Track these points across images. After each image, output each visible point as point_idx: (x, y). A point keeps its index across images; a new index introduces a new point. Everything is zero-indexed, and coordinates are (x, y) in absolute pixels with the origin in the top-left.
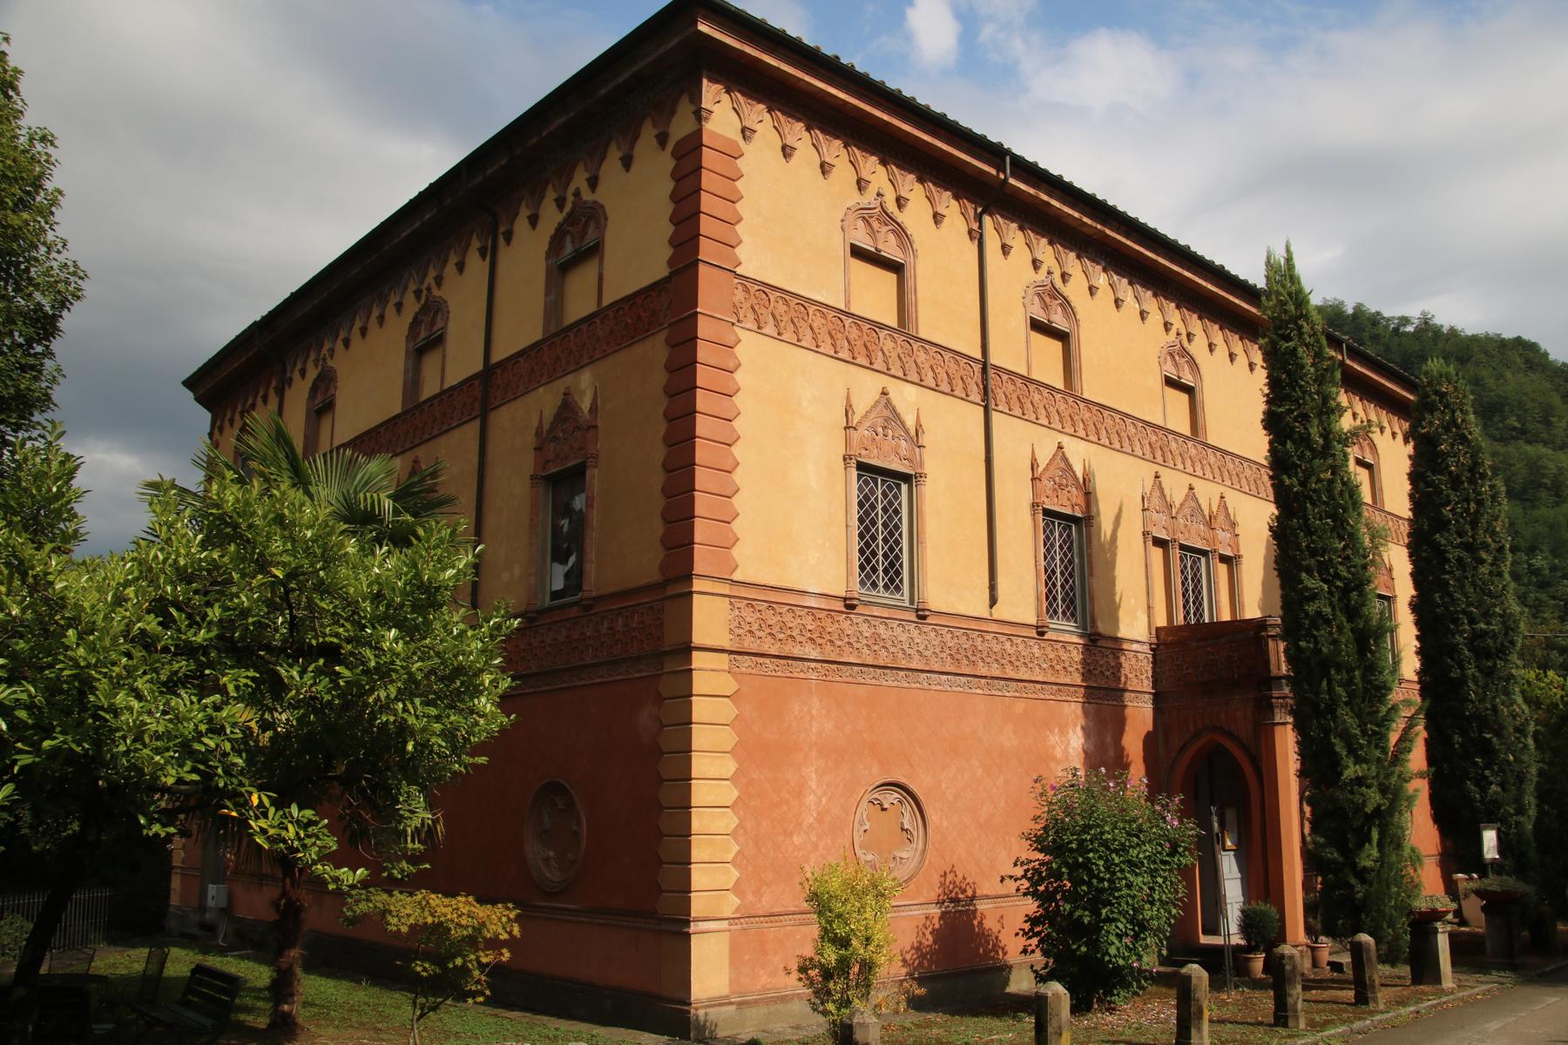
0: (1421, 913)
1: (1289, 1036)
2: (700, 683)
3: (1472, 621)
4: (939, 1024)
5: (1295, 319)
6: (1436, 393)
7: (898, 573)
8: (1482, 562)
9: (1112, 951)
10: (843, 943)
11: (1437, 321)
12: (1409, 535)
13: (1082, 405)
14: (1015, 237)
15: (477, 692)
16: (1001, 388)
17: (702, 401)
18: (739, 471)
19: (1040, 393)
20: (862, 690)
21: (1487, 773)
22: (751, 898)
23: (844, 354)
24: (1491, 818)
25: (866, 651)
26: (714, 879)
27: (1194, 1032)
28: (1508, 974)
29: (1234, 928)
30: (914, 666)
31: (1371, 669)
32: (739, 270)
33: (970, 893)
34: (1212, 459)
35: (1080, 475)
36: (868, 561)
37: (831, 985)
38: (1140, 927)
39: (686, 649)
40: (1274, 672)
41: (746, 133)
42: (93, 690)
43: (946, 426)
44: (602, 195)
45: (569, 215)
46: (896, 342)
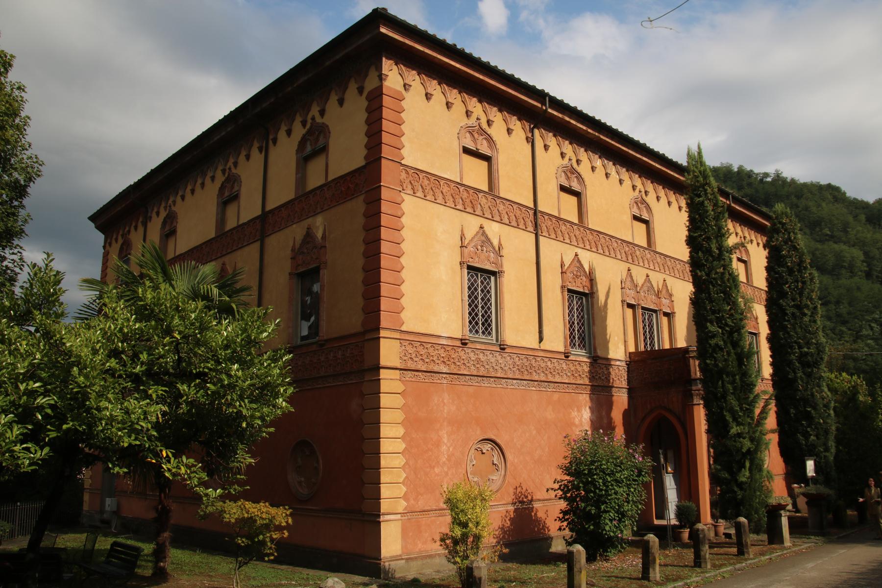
0: (773, 506)
1: (702, 572)
2: (384, 386)
3: (800, 347)
4: (514, 569)
5: (703, 186)
6: (780, 223)
7: (489, 325)
8: (805, 315)
9: (607, 528)
10: (465, 525)
11: (784, 175)
12: (767, 300)
13: (588, 232)
14: (552, 141)
15: (276, 395)
16: (544, 224)
17: (384, 233)
18: (404, 271)
19: (565, 225)
20: (471, 389)
21: (809, 429)
22: (412, 502)
23: (460, 207)
24: (811, 454)
25: (473, 368)
26: (393, 492)
27: (651, 570)
28: (820, 538)
29: (672, 516)
30: (498, 375)
31: (745, 374)
32: (403, 162)
33: (530, 498)
34: (659, 260)
35: (587, 270)
36: (473, 319)
37: (458, 548)
38: (622, 515)
39: (377, 368)
40: (693, 376)
41: (406, 87)
42: (89, 399)
43: (515, 245)
44: (326, 120)
46: (486, 200)
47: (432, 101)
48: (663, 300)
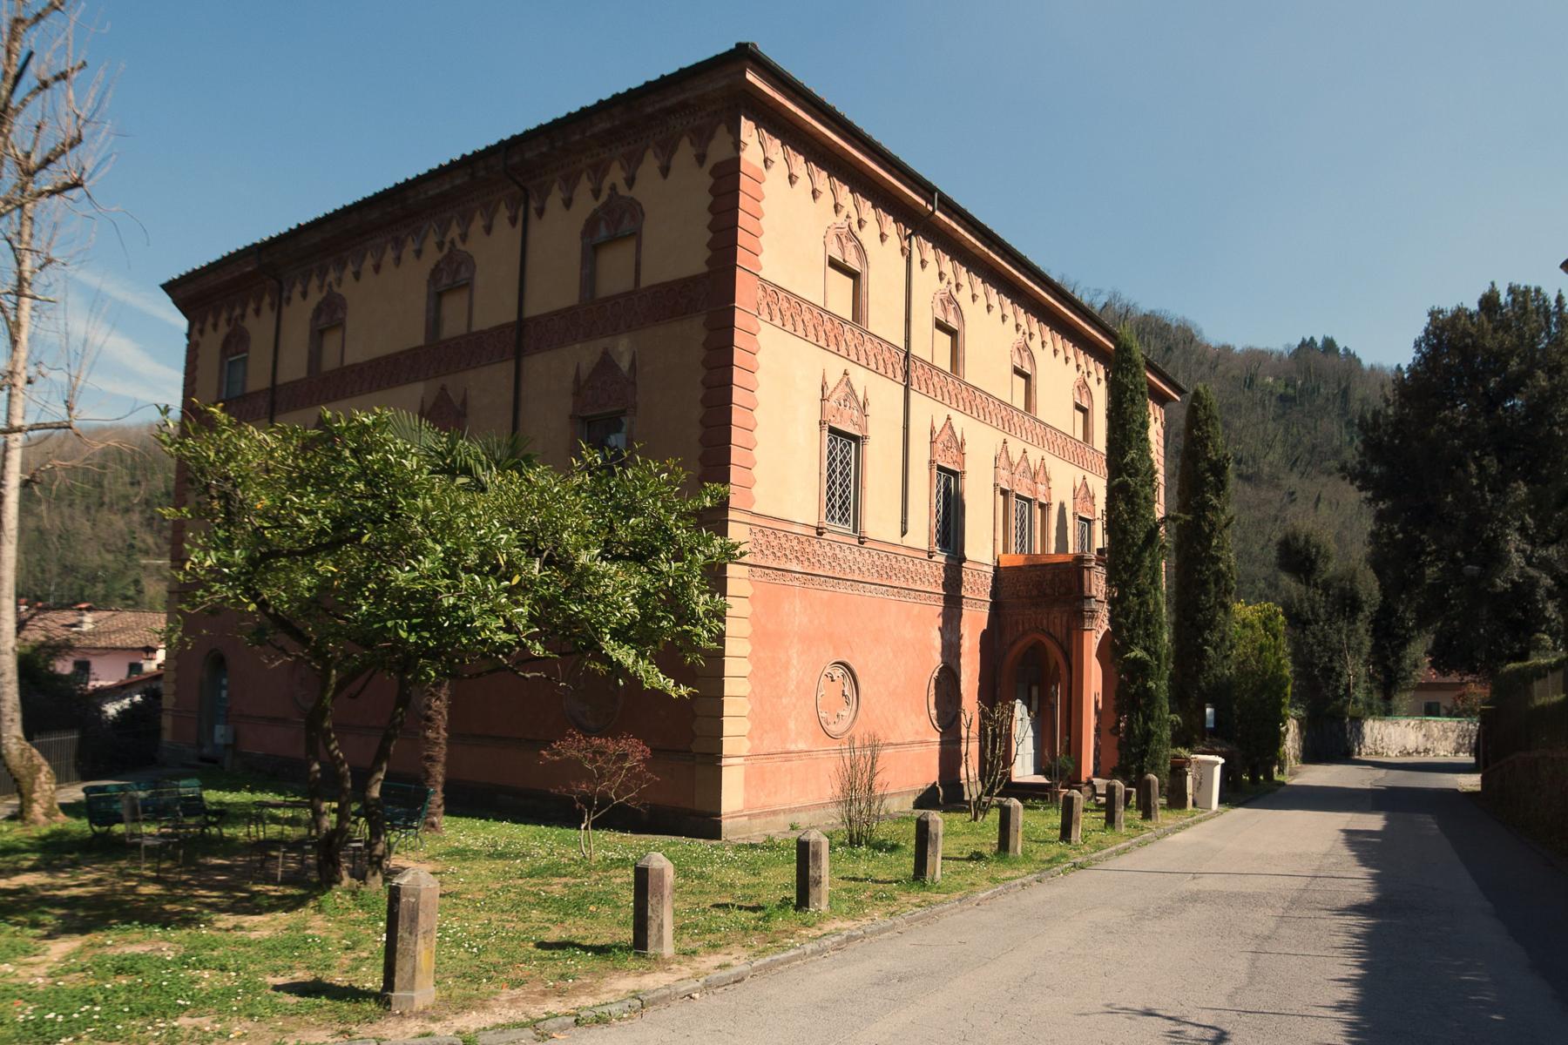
44: (638, 193)
45: (605, 204)
47: (819, 201)
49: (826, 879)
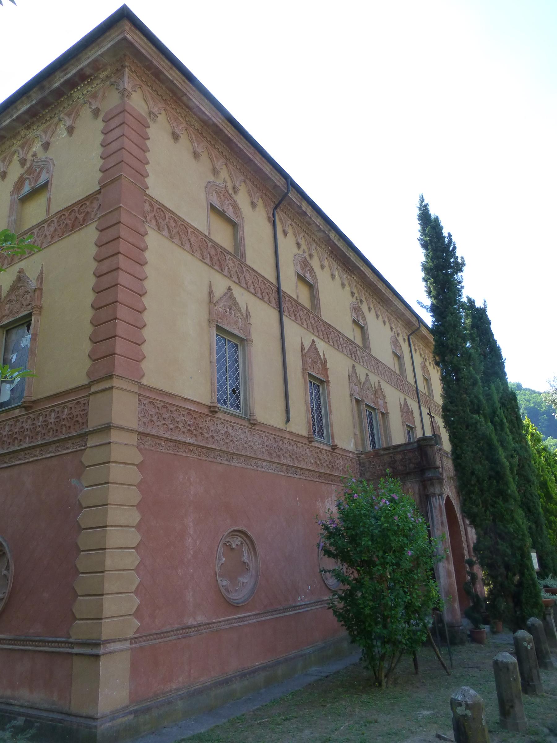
35: (407, 277)
43: (262, 317)
48: (379, 400)
49: (8, 552)
